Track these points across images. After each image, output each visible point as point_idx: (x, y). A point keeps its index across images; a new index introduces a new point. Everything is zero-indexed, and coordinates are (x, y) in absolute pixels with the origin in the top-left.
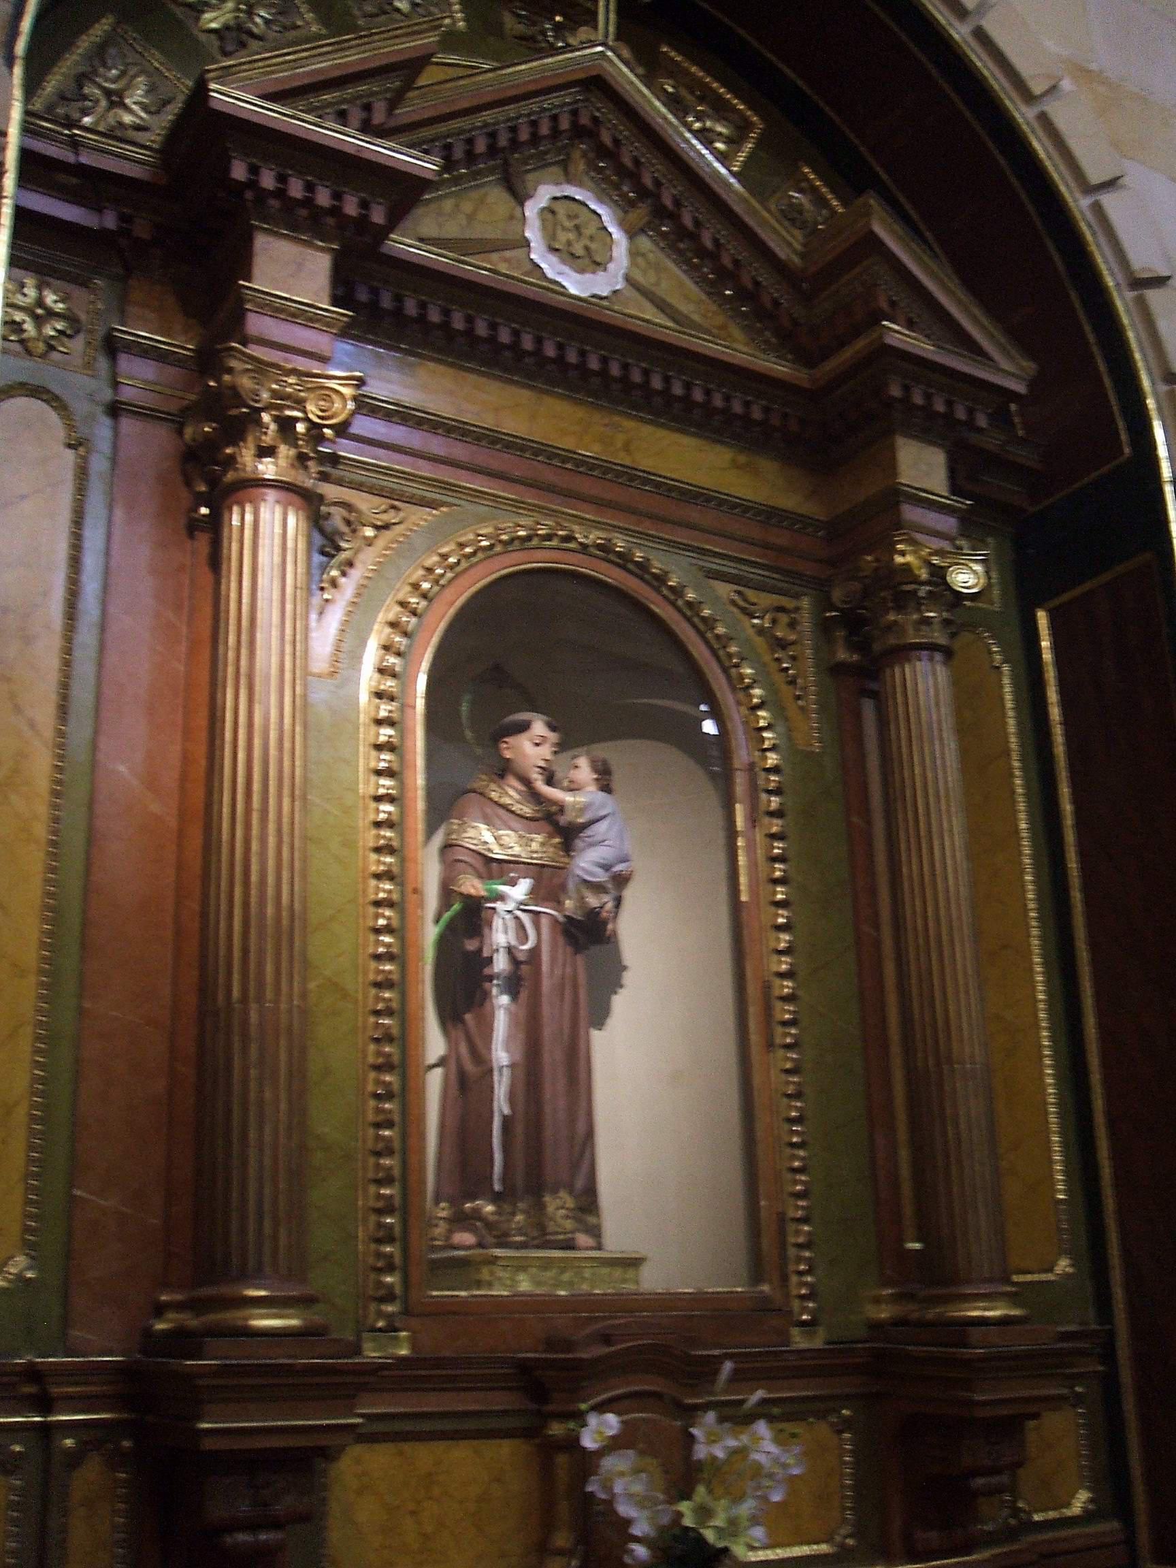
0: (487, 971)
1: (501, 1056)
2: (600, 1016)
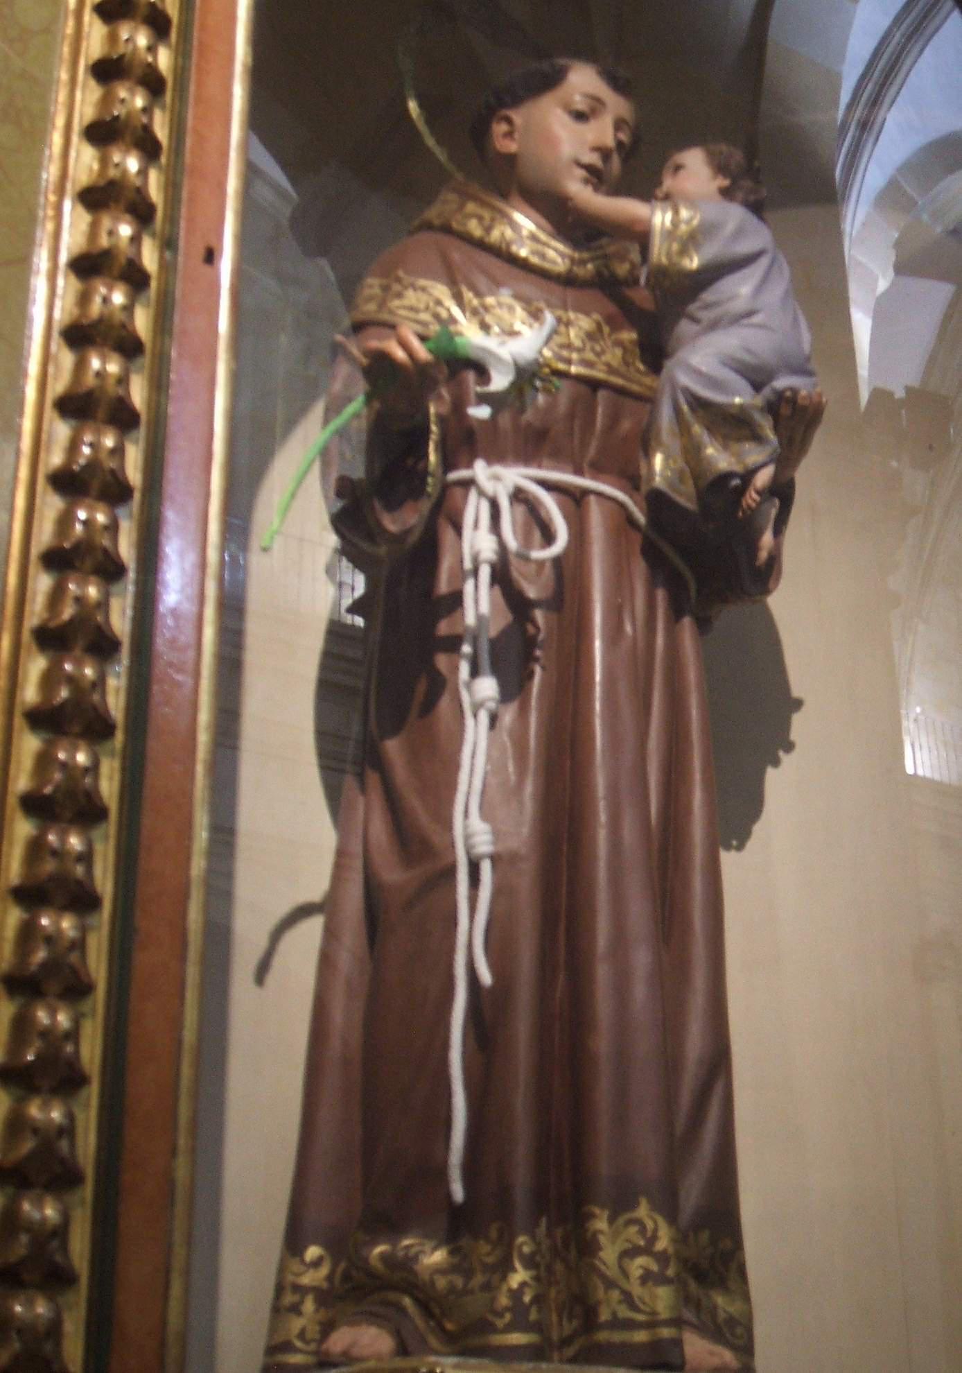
0: (444, 628)
1: (473, 829)
2: (738, 815)
